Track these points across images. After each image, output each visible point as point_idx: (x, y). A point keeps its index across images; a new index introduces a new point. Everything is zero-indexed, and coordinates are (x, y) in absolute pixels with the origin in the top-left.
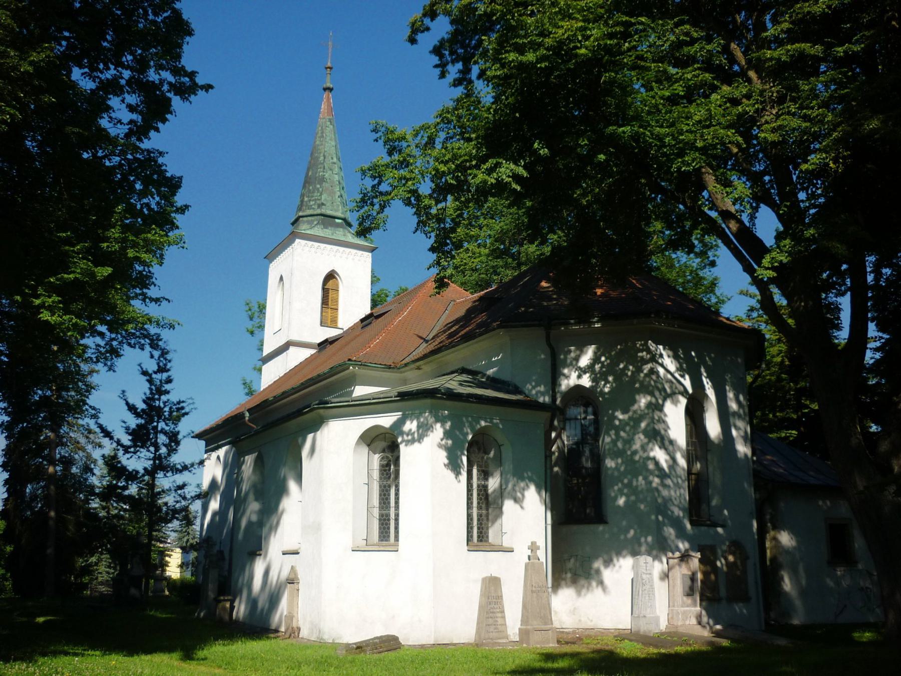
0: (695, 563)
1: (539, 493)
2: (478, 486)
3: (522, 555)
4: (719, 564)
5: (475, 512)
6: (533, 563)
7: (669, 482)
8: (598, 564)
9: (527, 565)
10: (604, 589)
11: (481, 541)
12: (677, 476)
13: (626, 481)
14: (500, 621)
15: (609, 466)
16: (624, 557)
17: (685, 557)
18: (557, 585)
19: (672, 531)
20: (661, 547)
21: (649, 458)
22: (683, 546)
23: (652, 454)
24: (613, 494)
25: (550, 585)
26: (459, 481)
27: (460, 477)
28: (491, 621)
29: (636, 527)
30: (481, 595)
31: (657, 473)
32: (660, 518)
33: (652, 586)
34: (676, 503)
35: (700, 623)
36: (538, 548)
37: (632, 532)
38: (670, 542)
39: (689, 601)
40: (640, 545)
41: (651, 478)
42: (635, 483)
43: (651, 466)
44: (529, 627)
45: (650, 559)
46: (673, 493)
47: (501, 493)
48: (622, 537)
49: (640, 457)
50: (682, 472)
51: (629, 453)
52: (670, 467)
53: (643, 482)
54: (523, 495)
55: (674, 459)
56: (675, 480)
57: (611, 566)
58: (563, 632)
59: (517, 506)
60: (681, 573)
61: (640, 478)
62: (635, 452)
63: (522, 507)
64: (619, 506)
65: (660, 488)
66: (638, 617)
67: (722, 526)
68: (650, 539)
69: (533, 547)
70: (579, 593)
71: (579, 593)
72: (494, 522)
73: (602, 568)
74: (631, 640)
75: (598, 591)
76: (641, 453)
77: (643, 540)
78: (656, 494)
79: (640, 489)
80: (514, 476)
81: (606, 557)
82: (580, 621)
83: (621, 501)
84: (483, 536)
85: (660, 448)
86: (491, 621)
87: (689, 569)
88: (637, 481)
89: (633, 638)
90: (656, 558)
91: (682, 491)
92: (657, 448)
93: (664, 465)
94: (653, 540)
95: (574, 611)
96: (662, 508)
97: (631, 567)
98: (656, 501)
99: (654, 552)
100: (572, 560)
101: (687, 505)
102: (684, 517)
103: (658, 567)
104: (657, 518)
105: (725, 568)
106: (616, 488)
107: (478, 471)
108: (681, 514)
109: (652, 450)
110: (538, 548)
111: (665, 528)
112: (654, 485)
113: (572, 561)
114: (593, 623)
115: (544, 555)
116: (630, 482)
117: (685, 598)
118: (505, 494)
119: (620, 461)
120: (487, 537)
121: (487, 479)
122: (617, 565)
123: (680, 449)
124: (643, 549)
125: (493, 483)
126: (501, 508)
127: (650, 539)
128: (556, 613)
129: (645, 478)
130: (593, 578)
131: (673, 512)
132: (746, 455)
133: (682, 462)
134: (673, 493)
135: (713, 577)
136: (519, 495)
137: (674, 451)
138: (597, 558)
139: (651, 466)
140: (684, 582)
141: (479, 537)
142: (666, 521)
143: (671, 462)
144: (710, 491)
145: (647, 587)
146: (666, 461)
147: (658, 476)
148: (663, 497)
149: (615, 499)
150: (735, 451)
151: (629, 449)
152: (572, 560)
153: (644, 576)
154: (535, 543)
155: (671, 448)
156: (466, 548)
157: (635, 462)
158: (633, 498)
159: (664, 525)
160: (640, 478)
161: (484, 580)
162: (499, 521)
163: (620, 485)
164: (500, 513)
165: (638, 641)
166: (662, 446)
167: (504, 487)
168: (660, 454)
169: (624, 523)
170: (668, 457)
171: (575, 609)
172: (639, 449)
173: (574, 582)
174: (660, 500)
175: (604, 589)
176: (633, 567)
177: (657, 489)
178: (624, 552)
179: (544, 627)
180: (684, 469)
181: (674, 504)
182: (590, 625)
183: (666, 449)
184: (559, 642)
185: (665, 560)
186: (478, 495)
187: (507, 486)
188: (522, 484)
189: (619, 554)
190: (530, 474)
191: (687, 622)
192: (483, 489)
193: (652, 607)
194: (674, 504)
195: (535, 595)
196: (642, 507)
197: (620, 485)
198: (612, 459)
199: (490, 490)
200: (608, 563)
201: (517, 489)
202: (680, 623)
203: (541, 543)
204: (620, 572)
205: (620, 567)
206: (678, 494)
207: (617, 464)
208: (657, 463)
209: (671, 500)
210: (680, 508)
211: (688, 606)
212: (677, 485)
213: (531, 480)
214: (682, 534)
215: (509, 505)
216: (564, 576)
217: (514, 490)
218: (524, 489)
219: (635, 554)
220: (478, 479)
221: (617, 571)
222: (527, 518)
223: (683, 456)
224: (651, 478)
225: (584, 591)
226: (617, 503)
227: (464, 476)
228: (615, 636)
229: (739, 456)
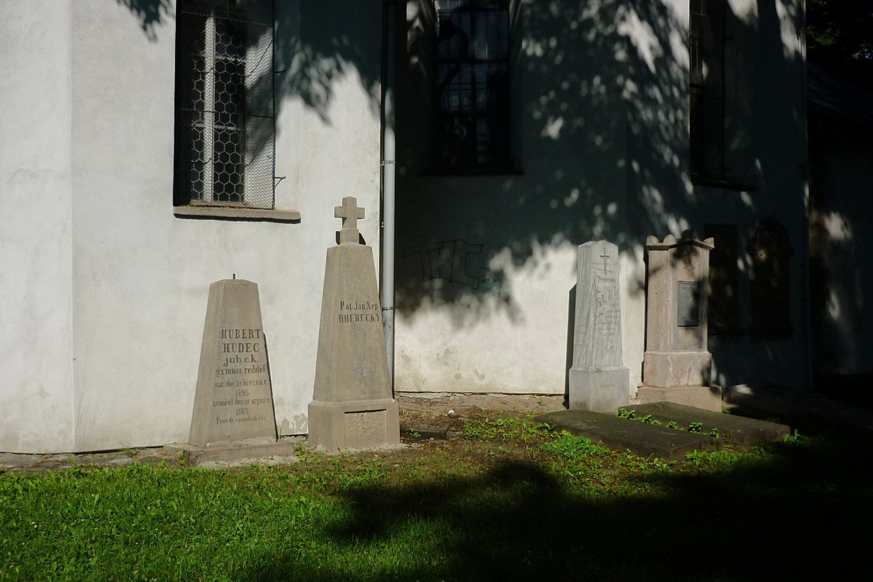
0: (702, 262)
1: (368, 87)
2: (218, 65)
3: (320, 230)
4: (740, 264)
5: (208, 126)
6: (345, 249)
7: (655, 92)
8: (501, 261)
9: (331, 253)
10: (514, 315)
11: (224, 198)
12: (673, 83)
13: (565, 85)
14: (254, 392)
15: (530, 52)
16: (557, 246)
17: (683, 250)
18: (408, 300)
19: (657, 195)
20: (632, 230)
21: (616, 37)
22: (677, 227)
23: (623, 29)
24: (537, 115)
25: (389, 301)
26: (154, 38)
27: (156, 27)
28: (228, 393)
29: (583, 183)
30: (207, 329)
31: (631, 69)
32: (636, 166)
33: (615, 306)
34: (667, 137)
35: (706, 383)
36: (360, 214)
37: (575, 195)
38: (654, 220)
39: (688, 337)
40: (592, 222)
41: (620, 80)
42: (584, 91)
43: (621, 55)
44: (331, 404)
45: (613, 249)
46: (661, 116)
47: (274, 86)
48: (554, 204)
49: (598, 35)
50: (681, 76)
51: (574, 25)
52: (657, 61)
53: (603, 89)
54: (328, 90)
55: (665, 45)
56: (667, 90)
57: (529, 264)
58: (420, 401)
59: (312, 117)
60: (675, 283)
61: (597, 80)
62: (589, 24)
63: (325, 119)
64: (549, 138)
65: (639, 105)
66: (586, 372)
67: (750, 190)
68: (612, 208)
69: (348, 212)
70: (458, 323)
71: (458, 323)
72: (256, 152)
73: (509, 270)
74: (576, 431)
75: (500, 319)
76: (600, 27)
77: (598, 210)
78: (630, 116)
79: (595, 102)
80: (305, 42)
81: (517, 246)
82: (458, 377)
83: (554, 129)
84: (230, 187)
85: (641, 18)
86: (228, 393)
87: (691, 273)
88: (590, 84)
89: (579, 424)
90: (625, 248)
91: (680, 114)
92: (633, 17)
93: (648, 57)
94: (618, 211)
95: (445, 357)
96: (641, 143)
97: (569, 267)
98: (629, 129)
99: (622, 238)
100: (441, 245)
101: (687, 143)
102: (681, 168)
103: (628, 268)
104: (629, 166)
105: (751, 275)
106: (544, 100)
107: (218, 28)
108: (676, 161)
109: (623, 19)
110: (360, 214)
111: (645, 190)
112: (626, 95)
113: (446, 254)
114: (484, 382)
115: (375, 228)
116: (575, 88)
117: (681, 332)
118: (285, 84)
119: (553, 43)
120: (241, 188)
121: (243, 54)
122: (542, 263)
123: (678, 26)
124: (598, 230)
125: (257, 62)
126: (274, 118)
127: (612, 208)
128: (407, 359)
129: (608, 81)
130: (488, 290)
131: (661, 156)
132: (797, 53)
133: (681, 54)
134: (661, 116)
135: (729, 291)
136: (317, 88)
137: (667, 30)
138: (498, 249)
139: (621, 55)
140: (680, 298)
141: (217, 188)
142: (647, 174)
143: (660, 52)
144: (727, 122)
145: (607, 307)
146: (651, 48)
147: (634, 79)
148: (642, 123)
149: (543, 123)
150: (781, 45)
151: (576, 17)
152: (441, 245)
153: (601, 285)
154: (354, 200)
155: (661, 22)
156: (171, 209)
157: (583, 44)
158: (579, 122)
159: (644, 181)
160: (597, 80)
161: (214, 287)
162: (268, 151)
163: (552, 94)
164: (271, 131)
165: (591, 434)
166: (645, 16)
167: (281, 68)
168: (638, 31)
169: (559, 175)
170: (655, 41)
171: (447, 352)
172: (597, 18)
173: (449, 297)
174: (636, 129)
175: (514, 315)
176: (576, 267)
177: (630, 105)
178: (557, 237)
179: (369, 404)
180: (684, 69)
181: (663, 141)
182: (479, 385)
183: (652, 24)
184: (405, 434)
185: (640, 254)
186: (218, 87)
187: (288, 65)
188: (326, 64)
189: (545, 240)
190: (345, 41)
191: (684, 381)
192: (231, 75)
193: (616, 350)
194: (663, 141)
195: (347, 325)
196: (599, 141)
197: (552, 94)
198: (537, 40)
199: (250, 80)
200: (522, 257)
201: (313, 72)
202: (669, 384)
203: (369, 203)
204: (546, 279)
205: (548, 267)
206: (669, 118)
207: (547, 49)
208: (632, 50)
209: (658, 130)
210: (675, 151)
211: (685, 348)
212: (670, 100)
213: (349, 56)
214: (676, 204)
215: (291, 112)
216: (427, 284)
217: (303, 74)
218: (329, 76)
219: (578, 238)
220: (219, 49)
221: (542, 277)
222: (335, 148)
223: (684, 42)
224: (620, 80)
225: (469, 317)
226: (544, 134)
227: (167, 29)
228: (537, 420)
229: (786, 54)
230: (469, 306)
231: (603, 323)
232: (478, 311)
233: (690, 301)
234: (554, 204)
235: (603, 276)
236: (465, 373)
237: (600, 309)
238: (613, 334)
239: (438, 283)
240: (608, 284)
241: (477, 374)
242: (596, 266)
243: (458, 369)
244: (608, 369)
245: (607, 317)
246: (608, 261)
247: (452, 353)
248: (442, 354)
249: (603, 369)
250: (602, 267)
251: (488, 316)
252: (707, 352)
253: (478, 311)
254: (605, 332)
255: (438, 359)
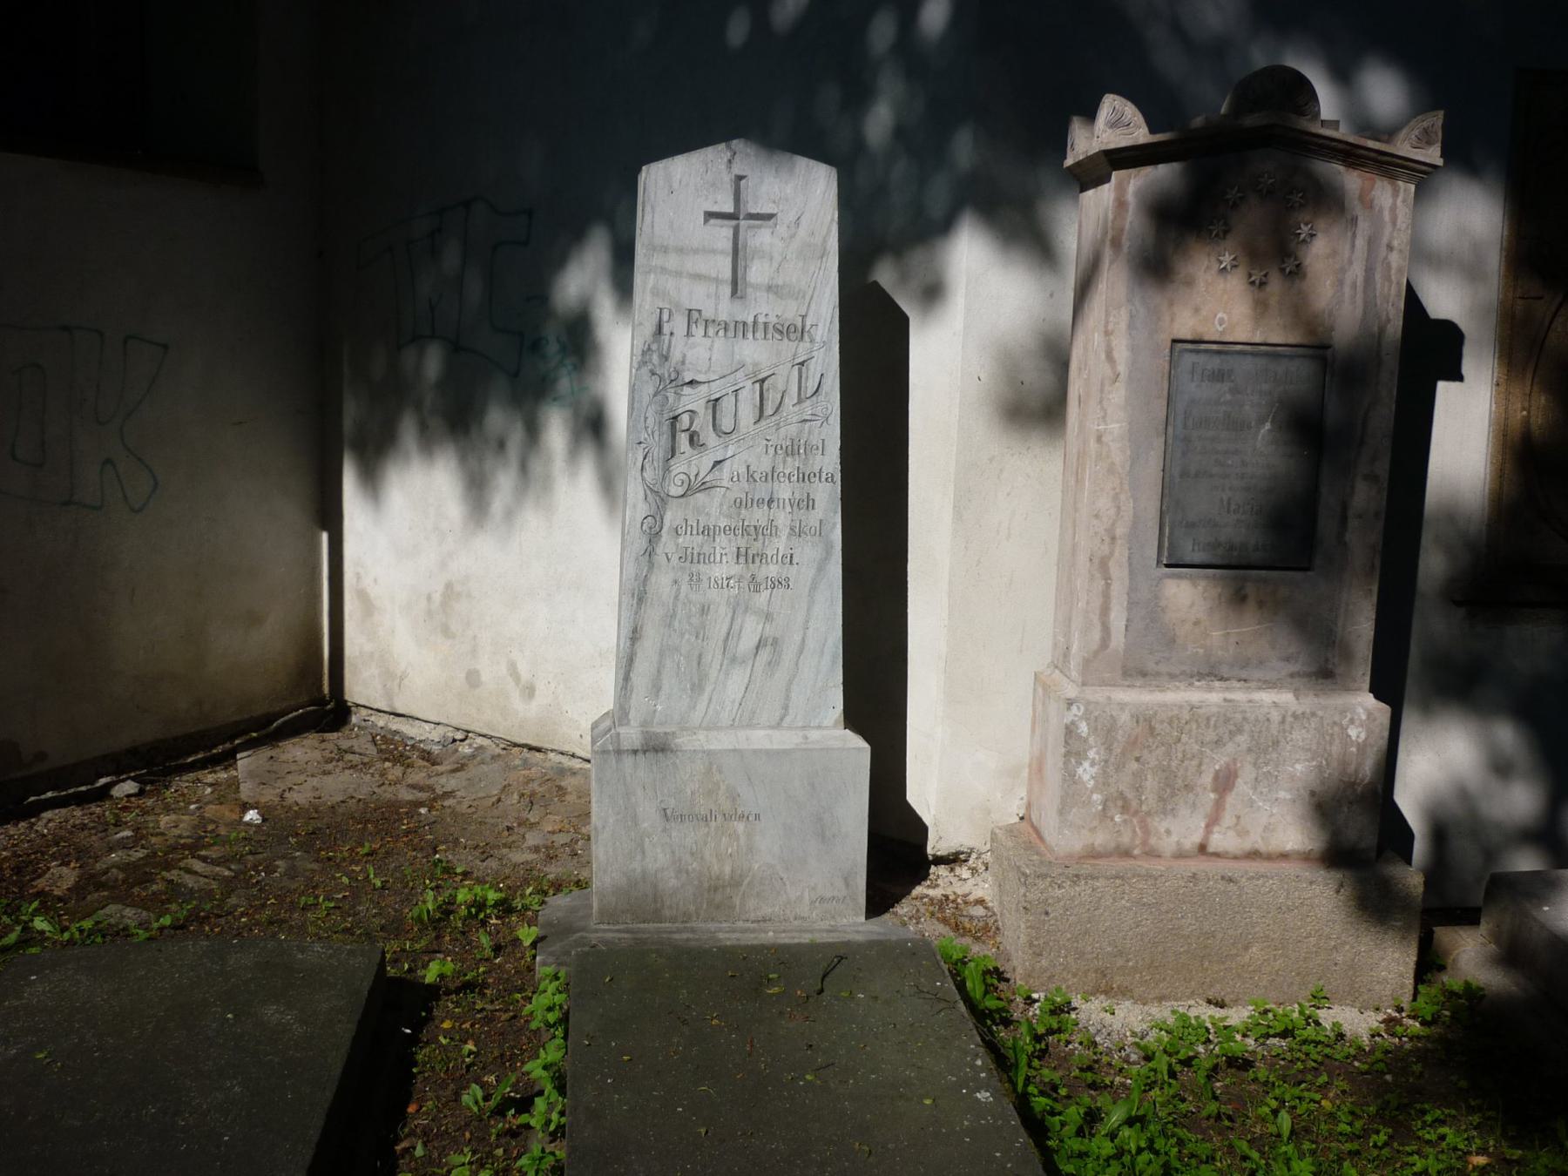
82: (473, 679)
171: (450, 593)
230: (502, 445)
231: (708, 532)
232: (524, 468)
233: (1261, 452)
234: (738, 30)
235: (725, 309)
236: (491, 671)
237: (689, 464)
238: (776, 583)
239: (433, 363)
240: (754, 351)
242: (672, 261)
244: (721, 741)
245: (739, 504)
246: (761, 238)
248: (437, 597)
249: (683, 741)
250: (724, 266)
251: (547, 485)
252: (1370, 700)
253: (524, 468)
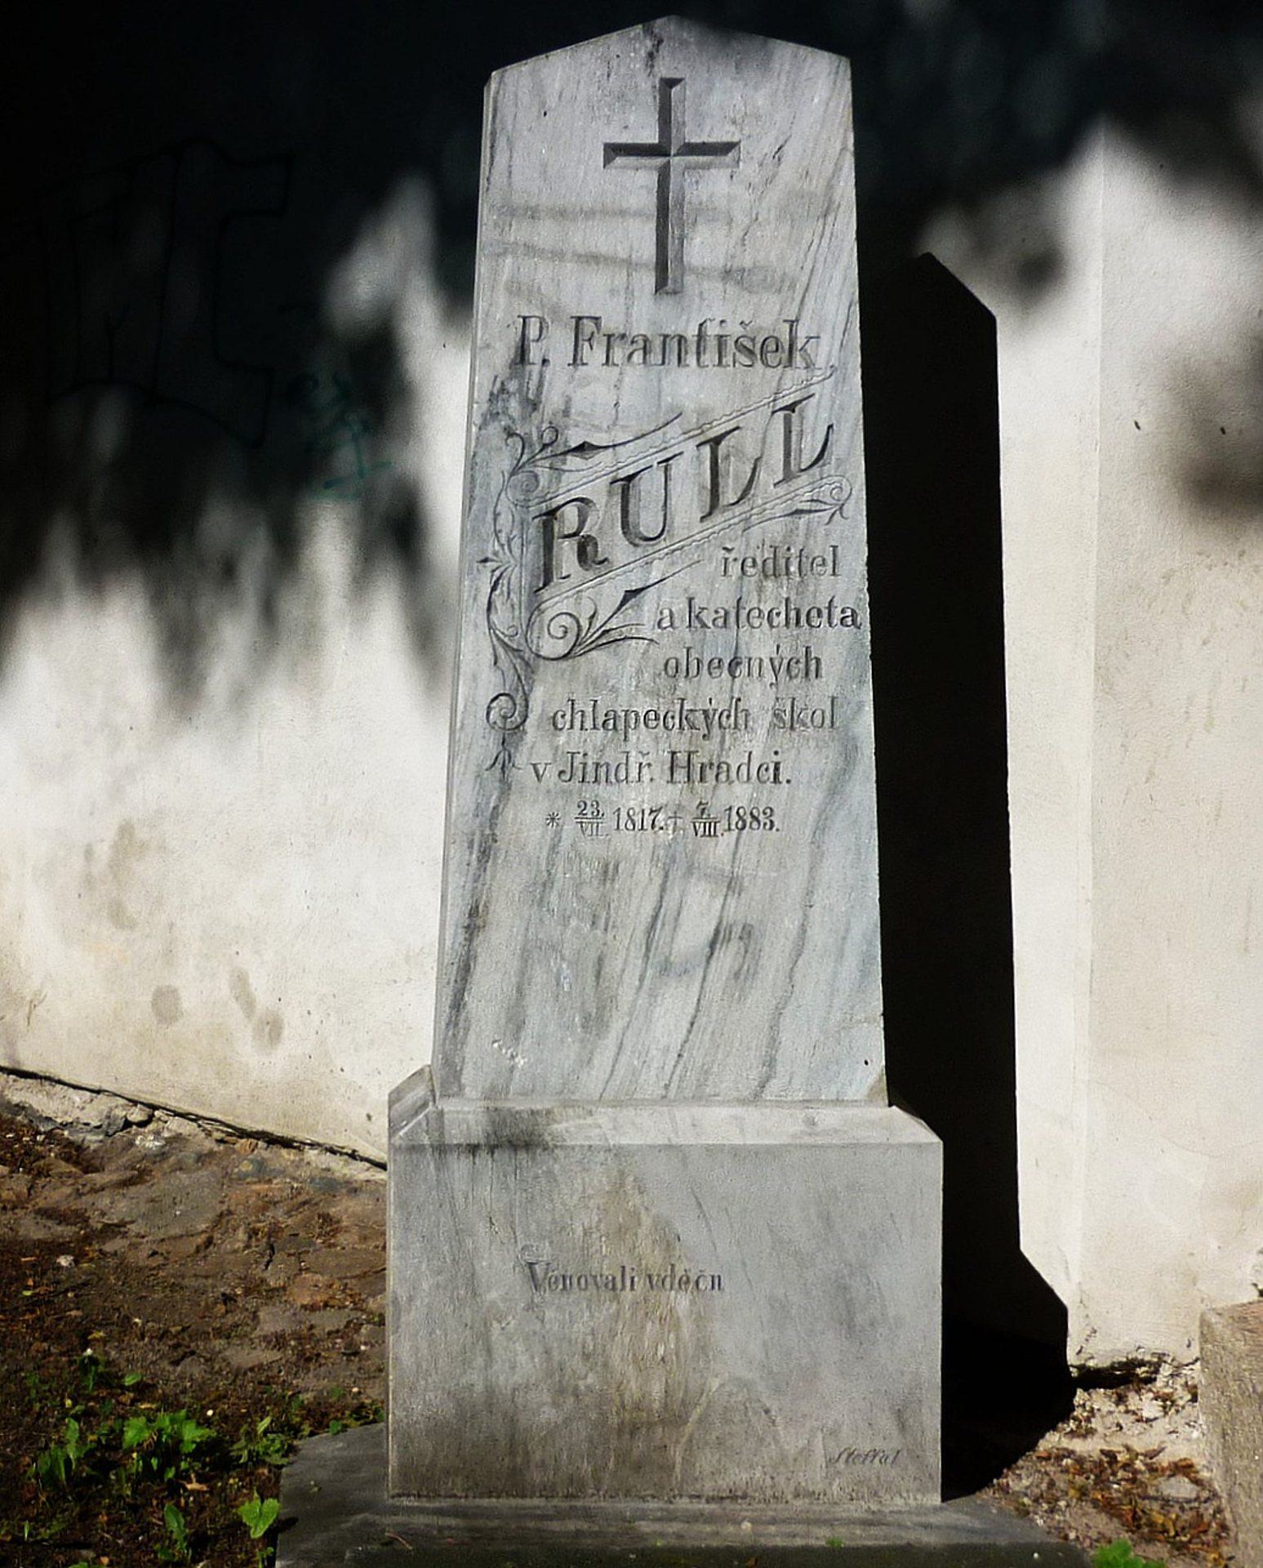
82: (165, 1005)
95: (116, 875)
171: (128, 843)
231: (614, 723)
232: (269, 612)
237: (577, 597)
241: (248, 1004)
242: (545, 234)
243: (169, 955)
244: (642, 1129)
245: (673, 670)
247: (144, 846)
248: (103, 851)
249: (567, 1128)
250: (642, 240)
251: (311, 639)
253: (269, 612)
254: (646, 791)
255: (89, 881)
